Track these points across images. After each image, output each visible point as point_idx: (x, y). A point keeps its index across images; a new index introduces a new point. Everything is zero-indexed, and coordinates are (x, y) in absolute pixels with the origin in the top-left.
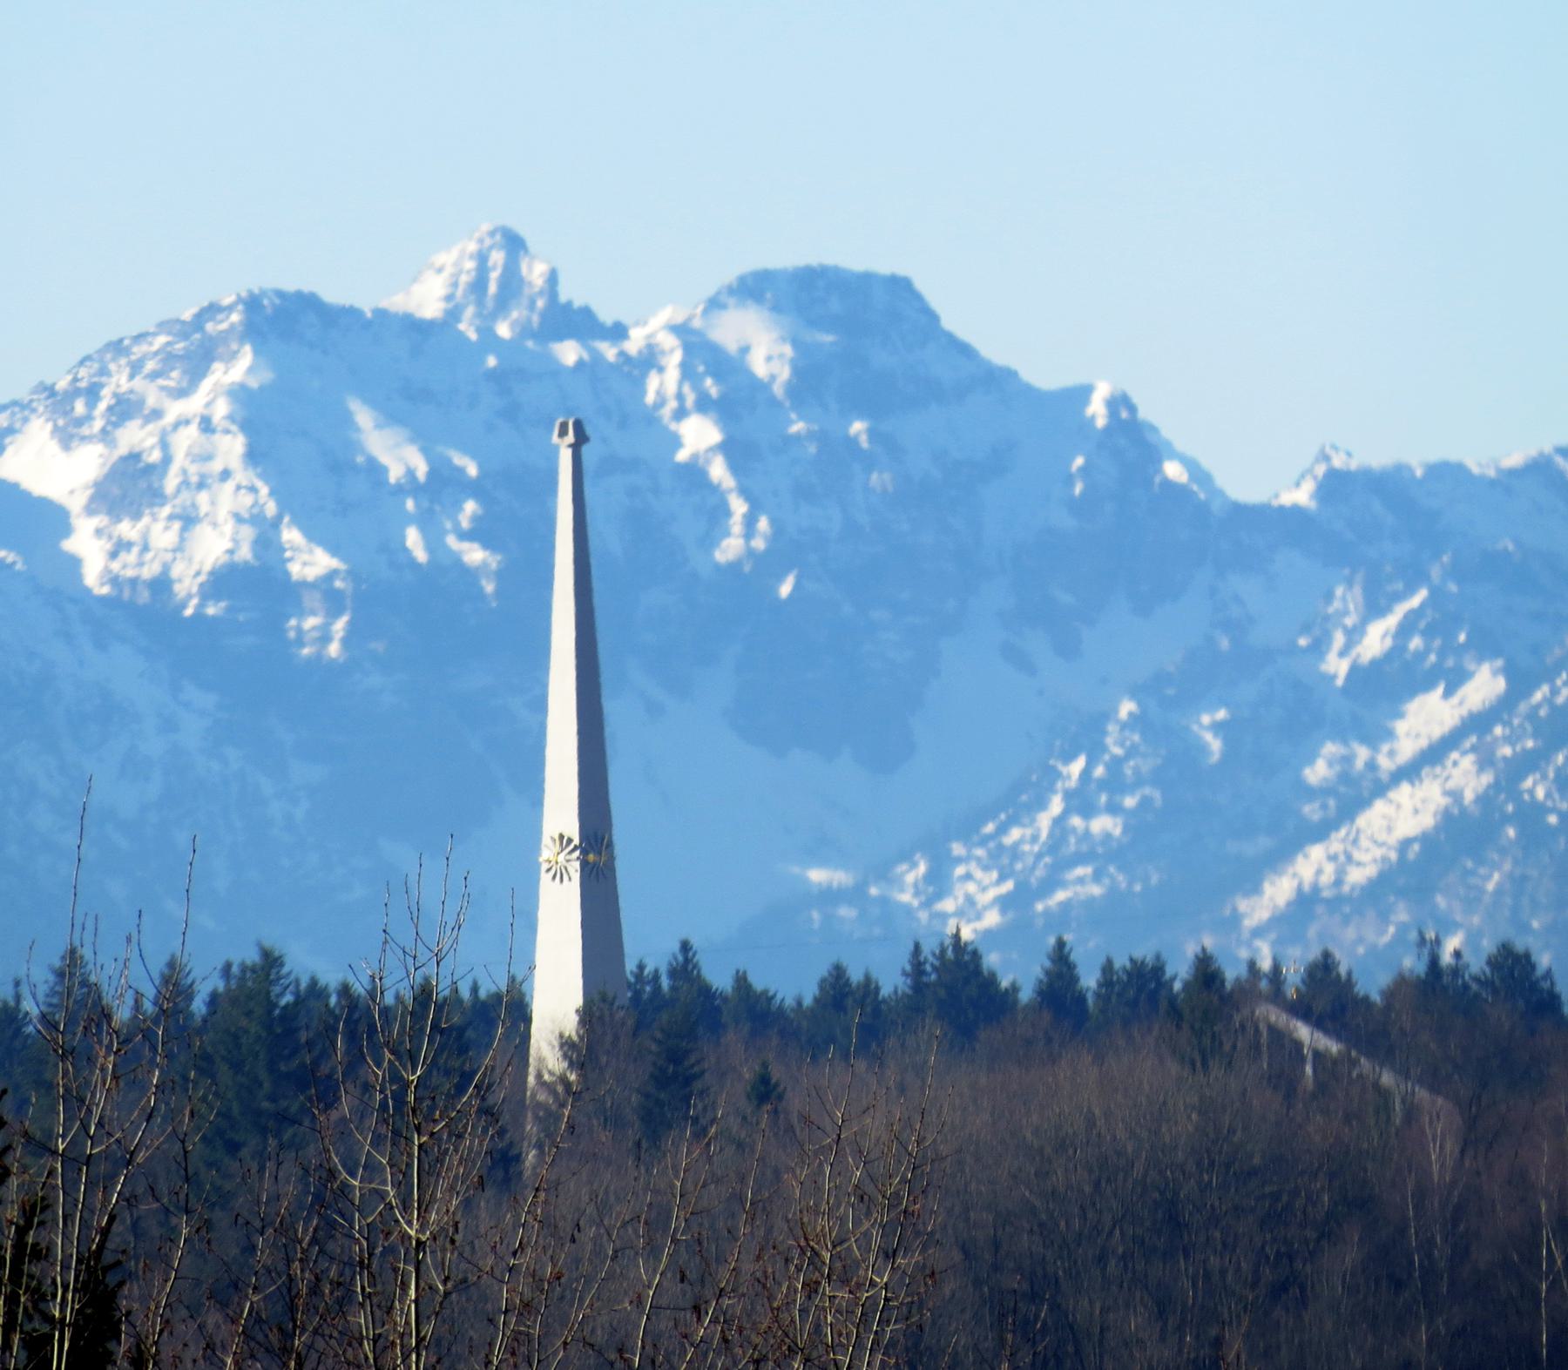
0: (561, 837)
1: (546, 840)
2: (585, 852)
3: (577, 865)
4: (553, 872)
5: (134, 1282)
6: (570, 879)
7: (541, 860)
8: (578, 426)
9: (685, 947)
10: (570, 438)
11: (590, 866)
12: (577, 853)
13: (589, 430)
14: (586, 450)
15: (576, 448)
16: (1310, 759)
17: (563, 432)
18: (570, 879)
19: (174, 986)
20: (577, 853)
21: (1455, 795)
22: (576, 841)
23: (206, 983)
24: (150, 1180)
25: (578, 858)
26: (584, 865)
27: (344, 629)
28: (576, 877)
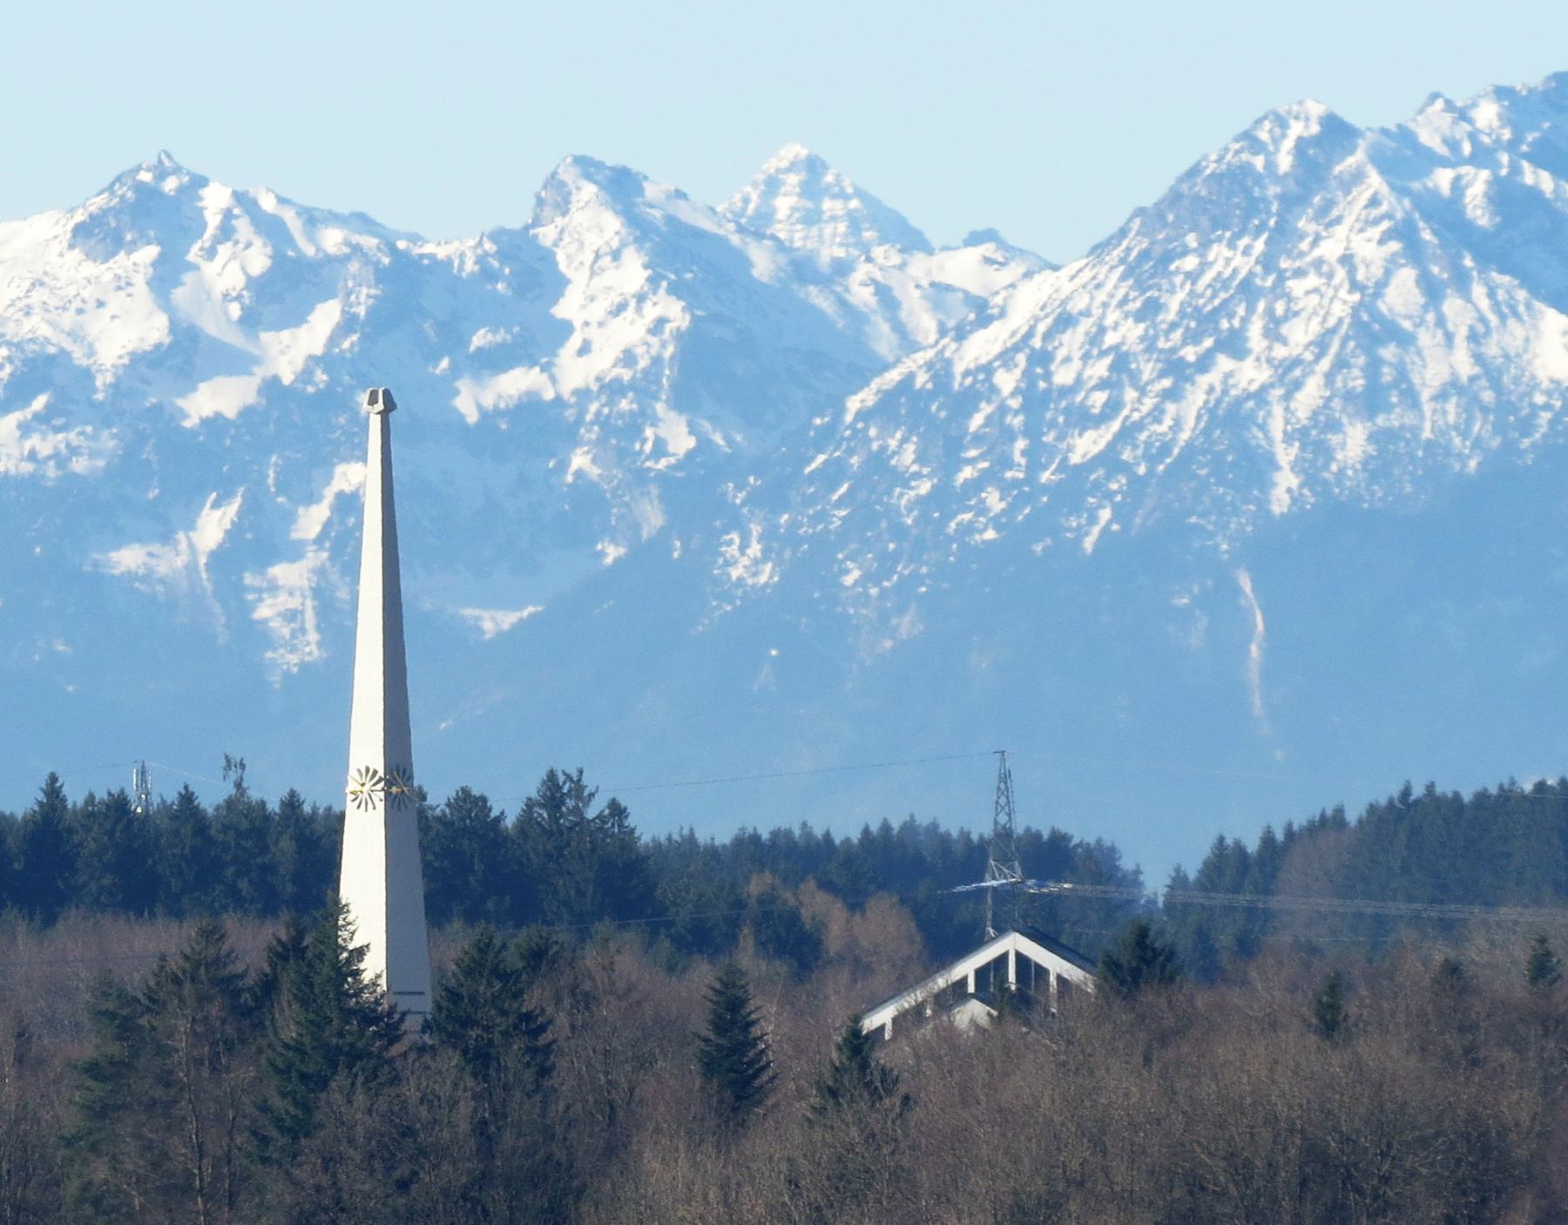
0: (368, 770)
1: (353, 773)
2: (389, 783)
3: (382, 795)
4: (357, 802)
5: (750, 1019)
6: (374, 808)
7: (348, 791)
8: (387, 393)
9: (912, 816)
10: (380, 406)
11: (393, 797)
12: (382, 784)
13: (396, 398)
14: (392, 416)
15: (384, 414)
16: (1185, 604)
17: (373, 401)
18: (374, 808)
19: (866, 831)
20: (382, 784)
21: (25, 417)
22: (381, 773)
23: (896, 825)
24: (667, 981)
25: (383, 789)
26: (388, 795)
27: (512, 624)
28: (381, 806)
